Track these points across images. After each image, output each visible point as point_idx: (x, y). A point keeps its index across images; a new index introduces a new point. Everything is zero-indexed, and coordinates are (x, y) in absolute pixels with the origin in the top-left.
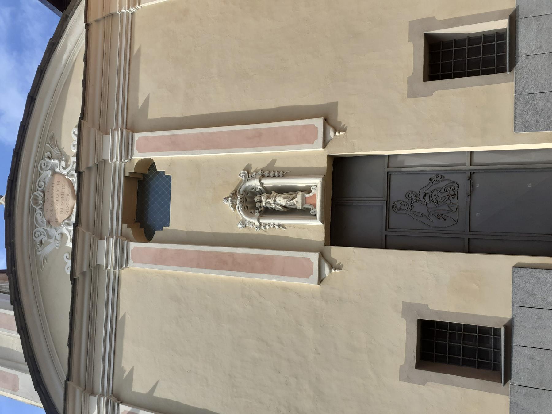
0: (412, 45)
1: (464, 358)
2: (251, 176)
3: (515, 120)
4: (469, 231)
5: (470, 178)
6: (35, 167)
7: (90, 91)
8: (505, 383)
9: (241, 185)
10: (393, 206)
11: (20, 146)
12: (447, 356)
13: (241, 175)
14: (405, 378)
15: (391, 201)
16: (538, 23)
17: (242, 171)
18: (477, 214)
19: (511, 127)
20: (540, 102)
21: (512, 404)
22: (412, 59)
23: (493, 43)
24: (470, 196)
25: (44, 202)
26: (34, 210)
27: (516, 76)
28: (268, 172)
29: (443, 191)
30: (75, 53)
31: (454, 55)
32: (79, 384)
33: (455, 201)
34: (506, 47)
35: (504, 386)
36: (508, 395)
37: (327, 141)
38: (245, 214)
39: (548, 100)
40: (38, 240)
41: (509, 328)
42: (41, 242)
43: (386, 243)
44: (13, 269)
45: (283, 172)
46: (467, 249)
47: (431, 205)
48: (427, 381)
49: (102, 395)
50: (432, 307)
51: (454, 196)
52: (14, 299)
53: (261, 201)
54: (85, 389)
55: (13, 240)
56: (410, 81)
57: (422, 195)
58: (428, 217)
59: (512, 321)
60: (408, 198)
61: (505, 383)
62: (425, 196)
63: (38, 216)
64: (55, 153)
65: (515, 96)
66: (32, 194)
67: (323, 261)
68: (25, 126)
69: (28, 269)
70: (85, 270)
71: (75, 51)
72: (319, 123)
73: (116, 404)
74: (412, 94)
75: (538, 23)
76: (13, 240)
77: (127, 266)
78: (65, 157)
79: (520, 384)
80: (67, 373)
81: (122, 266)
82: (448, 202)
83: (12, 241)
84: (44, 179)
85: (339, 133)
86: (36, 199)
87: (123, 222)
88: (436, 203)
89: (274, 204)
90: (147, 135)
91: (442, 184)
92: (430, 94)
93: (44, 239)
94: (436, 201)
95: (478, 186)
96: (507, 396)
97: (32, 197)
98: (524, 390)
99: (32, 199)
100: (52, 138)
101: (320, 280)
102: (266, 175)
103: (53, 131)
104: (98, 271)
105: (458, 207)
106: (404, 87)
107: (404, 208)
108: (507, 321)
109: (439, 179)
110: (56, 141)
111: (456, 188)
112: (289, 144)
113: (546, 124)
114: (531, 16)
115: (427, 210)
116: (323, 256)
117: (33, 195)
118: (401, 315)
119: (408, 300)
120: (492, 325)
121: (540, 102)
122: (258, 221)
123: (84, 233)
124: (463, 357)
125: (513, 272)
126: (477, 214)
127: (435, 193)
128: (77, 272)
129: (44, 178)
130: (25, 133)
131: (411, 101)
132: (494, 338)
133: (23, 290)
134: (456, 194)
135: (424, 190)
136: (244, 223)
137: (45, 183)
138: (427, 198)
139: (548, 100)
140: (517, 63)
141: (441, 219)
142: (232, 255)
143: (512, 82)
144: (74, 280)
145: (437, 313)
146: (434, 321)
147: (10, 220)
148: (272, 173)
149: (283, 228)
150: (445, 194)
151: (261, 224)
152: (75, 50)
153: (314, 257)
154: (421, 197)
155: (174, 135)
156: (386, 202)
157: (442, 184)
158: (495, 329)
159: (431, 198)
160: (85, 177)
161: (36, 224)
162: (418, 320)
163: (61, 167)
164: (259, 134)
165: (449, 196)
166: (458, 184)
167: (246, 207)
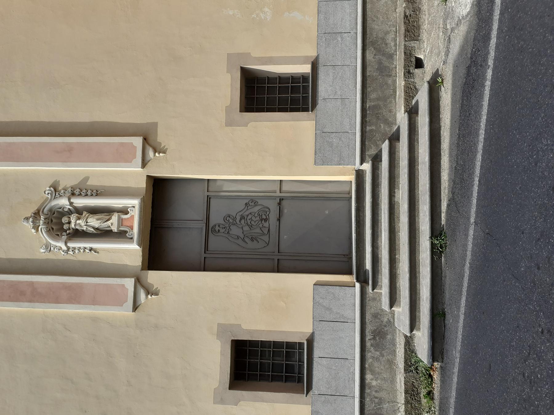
4: (279, 252)
5: (279, 204)
10: (212, 228)
17: (48, 188)
24: (279, 220)
27: (316, 116)
29: (256, 215)
33: (266, 225)
37: (146, 162)
41: (310, 341)
47: (246, 228)
50: (245, 326)
51: (266, 220)
53: (69, 223)
56: (228, 110)
57: (238, 218)
58: (243, 240)
60: (226, 221)
61: (312, 111)
62: (241, 219)
65: (316, 133)
67: (139, 286)
72: (138, 142)
74: (222, 329)
85: (159, 153)
88: (251, 226)
91: (256, 209)
92: (246, 125)
95: (286, 211)
101: (135, 307)
102: (77, 193)
105: (269, 230)
106: (222, 116)
111: (268, 213)
116: (139, 282)
119: (222, 321)
127: (250, 217)
135: (240, 214)
149: (95, 252)
150: (258, 218)
151: (68, 248)
164: (70, 148)
165: (262, 220)
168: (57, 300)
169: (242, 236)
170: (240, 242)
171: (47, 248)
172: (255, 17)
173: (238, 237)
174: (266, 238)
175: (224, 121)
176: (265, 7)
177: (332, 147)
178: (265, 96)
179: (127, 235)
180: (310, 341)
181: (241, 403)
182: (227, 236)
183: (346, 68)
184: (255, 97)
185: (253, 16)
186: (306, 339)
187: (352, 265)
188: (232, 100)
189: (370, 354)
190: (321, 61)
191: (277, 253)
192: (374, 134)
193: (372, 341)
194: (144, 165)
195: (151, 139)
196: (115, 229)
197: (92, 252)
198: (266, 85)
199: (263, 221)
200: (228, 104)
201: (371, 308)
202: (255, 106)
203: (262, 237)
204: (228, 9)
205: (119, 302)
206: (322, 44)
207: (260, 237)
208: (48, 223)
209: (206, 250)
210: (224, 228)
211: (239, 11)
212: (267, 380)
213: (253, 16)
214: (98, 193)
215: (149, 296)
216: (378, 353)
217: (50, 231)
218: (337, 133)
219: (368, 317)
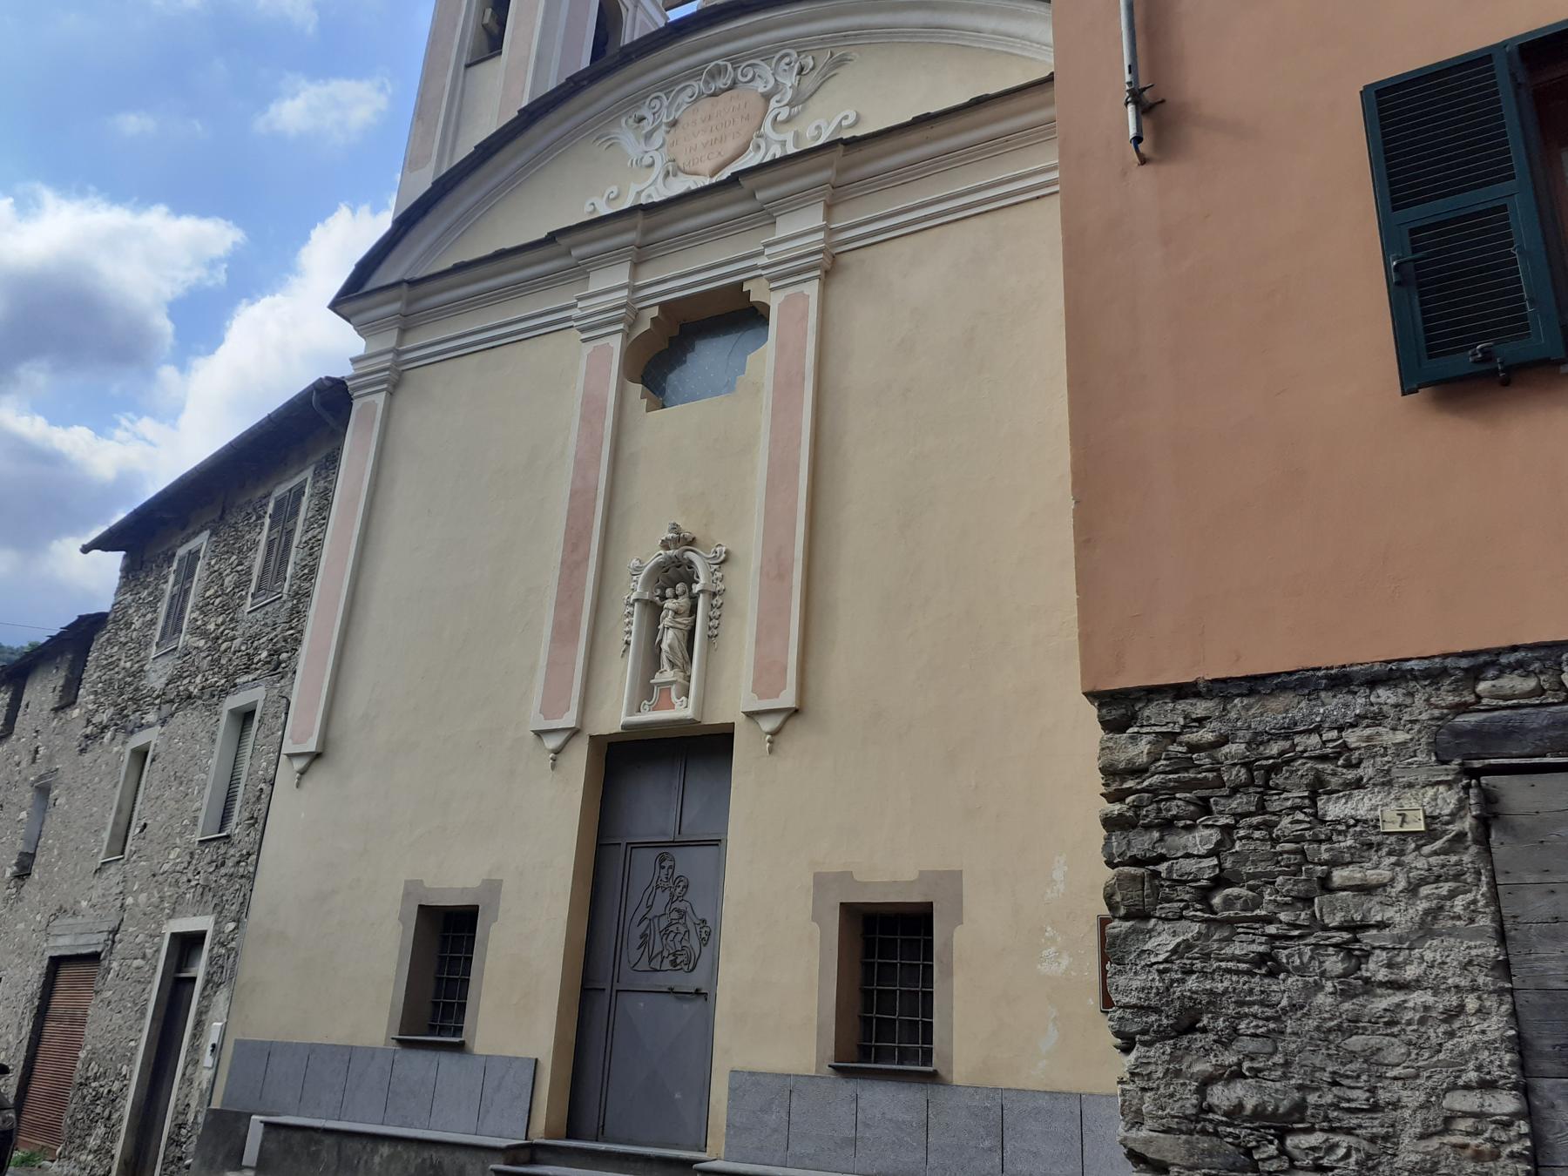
0: (912, 879)
1: (445, 980)
3: (749, 1072)
4: (617, 991)
5: (698, 992)
6: (782, 43)
7: (914, 136)
8: (399, 1041)
10: (667, 853)
13: (718, 549)
14: (411, 887)
15: (675, 849)
17: (724, 549)
20: (774, 1117)
21: (374, 1050)
23: (920, 1042)
24: (671, 991)
25: (714, 95)
26: (696, 75)
28: (719, 604)
29: (684, 943)
31: (910, 964)
33: (667, 965)
34: (913, 1065)
36: (385, 1045)
37: (756, 718)
38: (652, 568)
39: (775, 1130)
40: (645, 112)
41: (460, 1047)
42: (642, 119)
44: (585, 83)
45: (716, 635)
46: (586, 987)
47: (664, 923)
50: (494, 927)
51: (674, 963)
52: (576, 79)
53: (676, 597)
54: (405, 316)
55: (636, 57)
56: (845, 877)
57: (681, 906)
58: (644, 918)
59: (470, 1053)
61: (399, 1041)
62: (678, 911)
63: (689, 91)
64: (809, 82)
65: (790, 1075)
71: (1029, 48)
72: (788, 699)
74: (493, 887)
76: (636, 57)
77: (584, 341)
78: (798, 113)
79: (396, 1060)
81: (582, 331)
82: (665, 954)
83: (634, 57)
84: (759, 76)
85: (769, 741)
86: (719, 72)
87: (661, 305)
88: (666, 932)
90: (810, 314)
92: (816, 917)
93: (647, 126)
95: (686, 1006)
96: (383, 1043)
97: (720, 62)
98: (388, 1068)
99: (717, 65)
100: (841, 62)
101: (539, 734)
102: (714, 602)
103: (858, 56)
105: (656, 970)
106: (835, 865)
107: (664, 872)
108: (471, 1046)
110: (835, 75)
111: (686, 968)
113: (737, 1125)
114: (930, 1112)
115: (656, 916)
116: (575, 732)
117: (724, 63)
118: (485, 878)
120: (467, 1024)
121: (774, 1117)
122: (637, 600)
123: (634, 228)
125: (529, 1059)
126: (642, 1005)
127: (682, 930)
131: (809, 881)
133: (553, 117)
134: (678, 967)
135: (689, 910)
136: (638, 569)
137: (752, 80)
138: (675, 915)
139: (775, 1130)
140: (847, 1082)
144: (552, 238)
146: (475, 933)
147: (670, 34)
149: (624, 651)
151: (633, 605)
152: (1031, 46)
153: (569, 720)
156: (671, 840)
157: (695, 942)
158: (461, 1029)
159: (674, 922)
160: (735, 193)
161: (674, 92)
162: (478, 906)
164: (783, 575)
165: (674, 954)
170: (643, 910)
172: (1047, 934)
173: (650, 907)
174: (643, 965)
176: (1071, 959)
177: (761, 1110)
179: (645, 701)
180: (933, 1077)
181: (401, 927)
182: (654, 884)
183: (921, 1154)
185: (1049, 929)
186: (939, 1070)
187: (148, 1076)
188: (866, 884)
191: (617, 986)
194: (751, 715)
195: (796, 723)
196: (658, 678)
197: (625, 646)
199: (671, 958)
200: (857, 878)
201: (472, 1164)
202: (878, 936)
203: (645, 958)
204: (1066, 868)
206: (978, 1098)
208: (673, 562)
210: (667, 878)
212: (440, 970)
213: (1049, 929)
215: (551, 755)
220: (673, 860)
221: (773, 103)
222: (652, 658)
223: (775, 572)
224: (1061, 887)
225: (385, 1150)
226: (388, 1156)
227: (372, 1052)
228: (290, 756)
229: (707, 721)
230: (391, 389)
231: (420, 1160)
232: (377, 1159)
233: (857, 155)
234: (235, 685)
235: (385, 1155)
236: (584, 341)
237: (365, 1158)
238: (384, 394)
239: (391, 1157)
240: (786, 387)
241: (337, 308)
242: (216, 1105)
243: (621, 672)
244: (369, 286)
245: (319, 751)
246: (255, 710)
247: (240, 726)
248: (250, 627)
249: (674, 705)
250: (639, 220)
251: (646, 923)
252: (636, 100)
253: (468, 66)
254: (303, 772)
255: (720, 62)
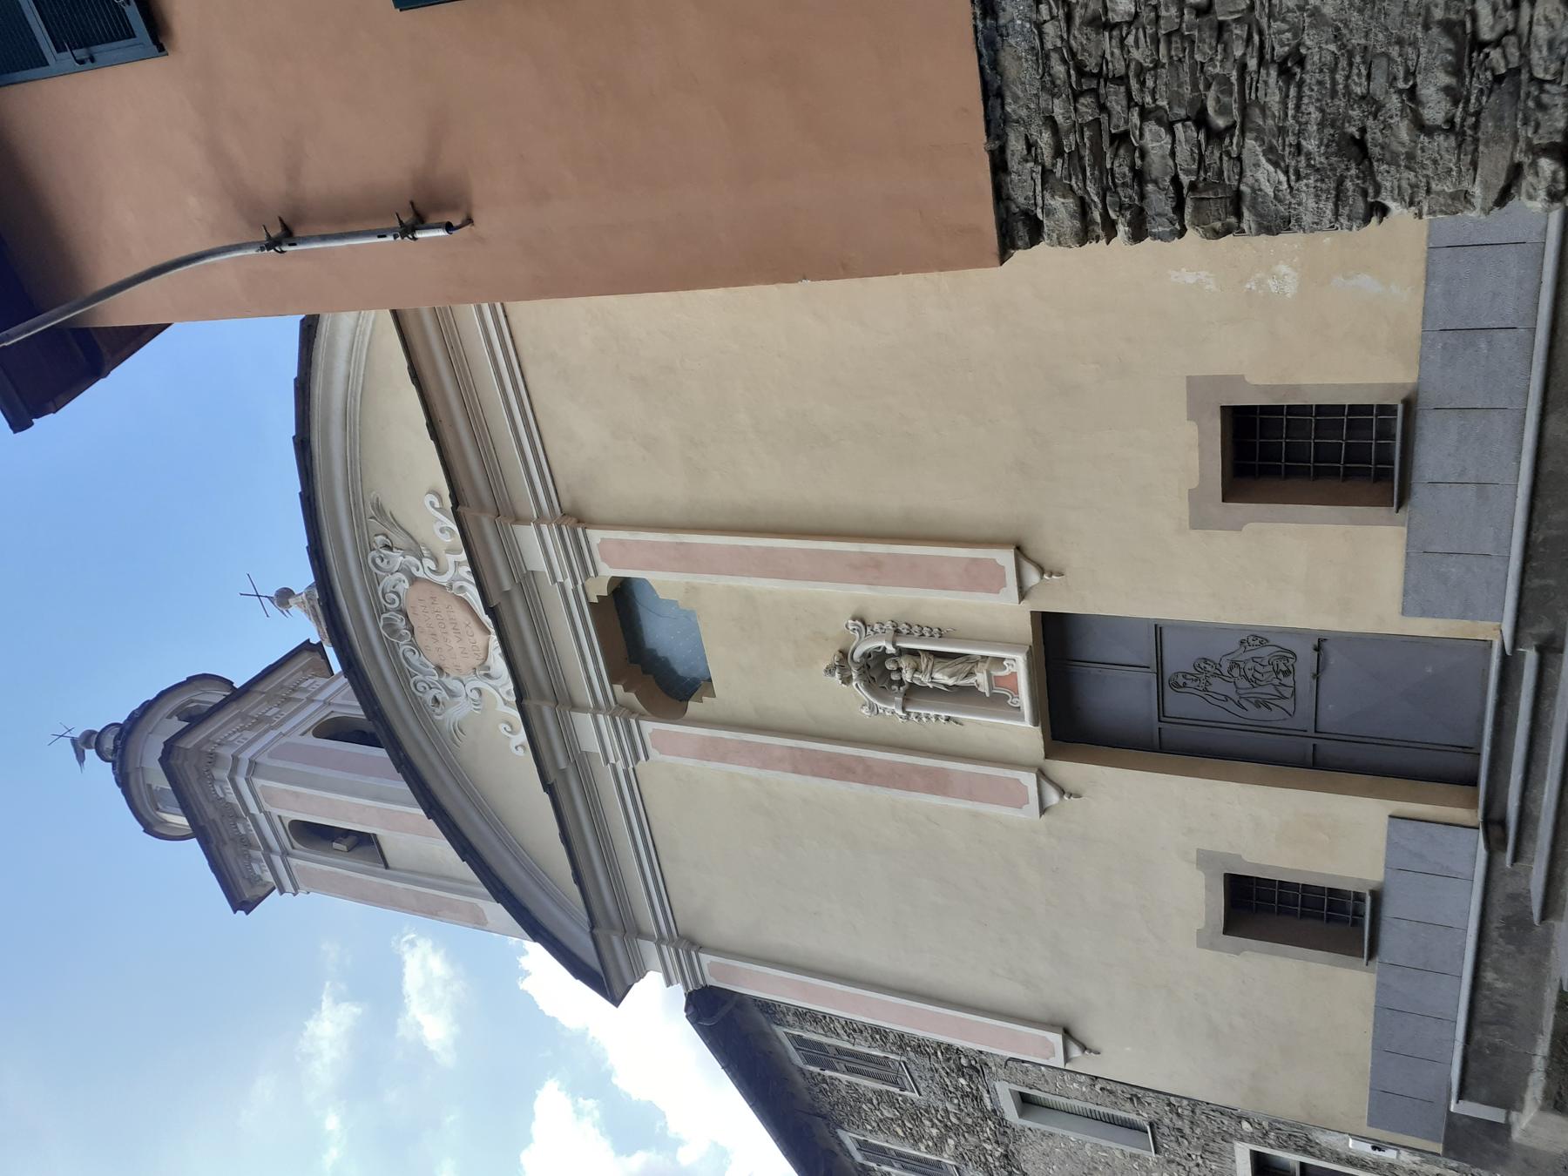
0: (1196, 428)
2: (872, 630)
4: (1316, 732)
5: (1318, 649)
6: (362, 566)
9: (854, 644)
11: (315, 537)
12: (1283, 465)
14: (1204, 941)
16: (1462, 422)
17: (851, 622)
18: (1330, 706)
19: (1397, 607)
22: (1196, 455)
24: (1317, 676)
25: (412, 631)
26: (394, 648)
27: (1410, 519)
28: (907, 627)
30: (365, 329)
32: (542, 697)
33: (1288, 681)
35: (1397, 512)
40: (429, 698)
41: (1377, 896)
42: (436, 700)
43: (1160, 738)
44: (402, 754)
45: (940, 629)
47: (1243, 683)
48: (1244, 950)
49: (541, 517)
50: (1247, 858)
51: (1286, 673)
53: (899, 670)
54: (625, 931)
56: (1195, 497)
58: (1239, 705)
60: (1199, 669)
61: (1400, 506)
62: (1231, 669)
63: (409, 655)
64: (398, 539)
66: (380, 618)
67: (1046, 785)
68: (309, 498)
69: (428, 750)
70: (507, 589)
72: (1006, 558)
73: (693, 953)
74: (1205, 860)
75: (1462, 422)
77: (647, 757)
78: (428, 549)
80: (585, 912)
81: (637, 759)
82: (1276, 682)
85: (1050, 576)
86: (389, 625)
87: (614, 679)
88: (1254, 682)
89: (932, 682)
91: (1265, 652)
94: (1254, 679)
95: (1332, 661)
97: (381, 624)
100: (379, 508)
102: (905, 631)
103: (374, 493)
104: (532, 579)
109: (1257, 642)
110: (392, 515)
112: (945, 588)
116: (1042, 774)
118: (1195, 865)
119: (1207, 847)
120: (1350, 887)
121: (1453, 570)
122: (903, 709)
124: (1304, 907)
126: (1330, 706)
127: (1250, 665)
128: (486, 573)
129: (393, 584)
130: (315, 509)
131: (1195, 534)
132: (1376, 443)
133: (434, 785)
134: (1291, 669)
136: (872, 707)
138: (1236, 672)
141: (1263, 708)
142: (860, 759)
143: (1403, 525)
144: (548, 788)
145: (1258, 866)
148: (916, 628)
150: (1269, 668)
151: (909, 714)
153: (1029, 780)
154: (1225, 671)
155: (682, 544)
157: (1265, 652)
160: (504, 612)
163: (426, 569)
164: (876, 563)
165: (1277, 673)
166: (1295, 655)
167: (871, 680)
168: (908, 786)
169: (1236, 698)
171: (873, 710)
172: (1253, 288)
175: (1186, 517)
178: (1283, 467)
179: (1009, 702)
182: (1202, 694)
184: (1259, 465)
185: (1248, 286)
189: (1495, 947)
190: (1426, 400)
191: (1311, 733)
192: (1552, 594)
193: (1502, 931)
194: (1023, 593)
195: (1031, 548)
198: (1325, 912)
199: (1281, 676)
200: (1195, 485)
204: (1184, 270)
205: (1019, 802)
207: (1276, 702)
208: (864, 672)
209: (1161, 715)
211: (1212, 275)
214: (942, 635)
216: (1512, 947)
217: (870, 684)
218: (1461, 556)
219: (1497, 897)
220: (1177, 674)
221: (419, 574)
222: (963, 695)
223: (871, 571)
224: (1203, 274)
225: (1489, 976)
226: (1496, 973)
227: (1382, 988)
228: (1067, 1059)
229: (1030, 640)
230: (695, 948)
231: (1501, 940)
232: (1499, 985)
233: (468, 494)
234: (994, 1111)
235: (1495, 976)
236: (647, 757)
237: (1498, 997)
238: (702, 955)
239: (1497, 970)
240: (687, 561)
241: (618, 997)
242: (1439, 1148)
243: (978, 726)
244: (596, 965)
245: (1061, 1031)
246: (1020, 1093)
247: (1036, 1107)
248: (934, 1093)
249: (1012, 673)
250: (530, 704)
251: (1244, 703)
252: (417, 706)
253: (387, 867)
254: (1084, 1048)
255: (381, 624)
